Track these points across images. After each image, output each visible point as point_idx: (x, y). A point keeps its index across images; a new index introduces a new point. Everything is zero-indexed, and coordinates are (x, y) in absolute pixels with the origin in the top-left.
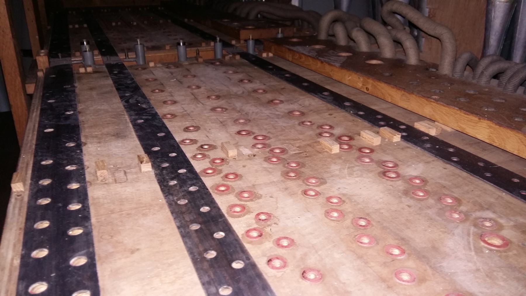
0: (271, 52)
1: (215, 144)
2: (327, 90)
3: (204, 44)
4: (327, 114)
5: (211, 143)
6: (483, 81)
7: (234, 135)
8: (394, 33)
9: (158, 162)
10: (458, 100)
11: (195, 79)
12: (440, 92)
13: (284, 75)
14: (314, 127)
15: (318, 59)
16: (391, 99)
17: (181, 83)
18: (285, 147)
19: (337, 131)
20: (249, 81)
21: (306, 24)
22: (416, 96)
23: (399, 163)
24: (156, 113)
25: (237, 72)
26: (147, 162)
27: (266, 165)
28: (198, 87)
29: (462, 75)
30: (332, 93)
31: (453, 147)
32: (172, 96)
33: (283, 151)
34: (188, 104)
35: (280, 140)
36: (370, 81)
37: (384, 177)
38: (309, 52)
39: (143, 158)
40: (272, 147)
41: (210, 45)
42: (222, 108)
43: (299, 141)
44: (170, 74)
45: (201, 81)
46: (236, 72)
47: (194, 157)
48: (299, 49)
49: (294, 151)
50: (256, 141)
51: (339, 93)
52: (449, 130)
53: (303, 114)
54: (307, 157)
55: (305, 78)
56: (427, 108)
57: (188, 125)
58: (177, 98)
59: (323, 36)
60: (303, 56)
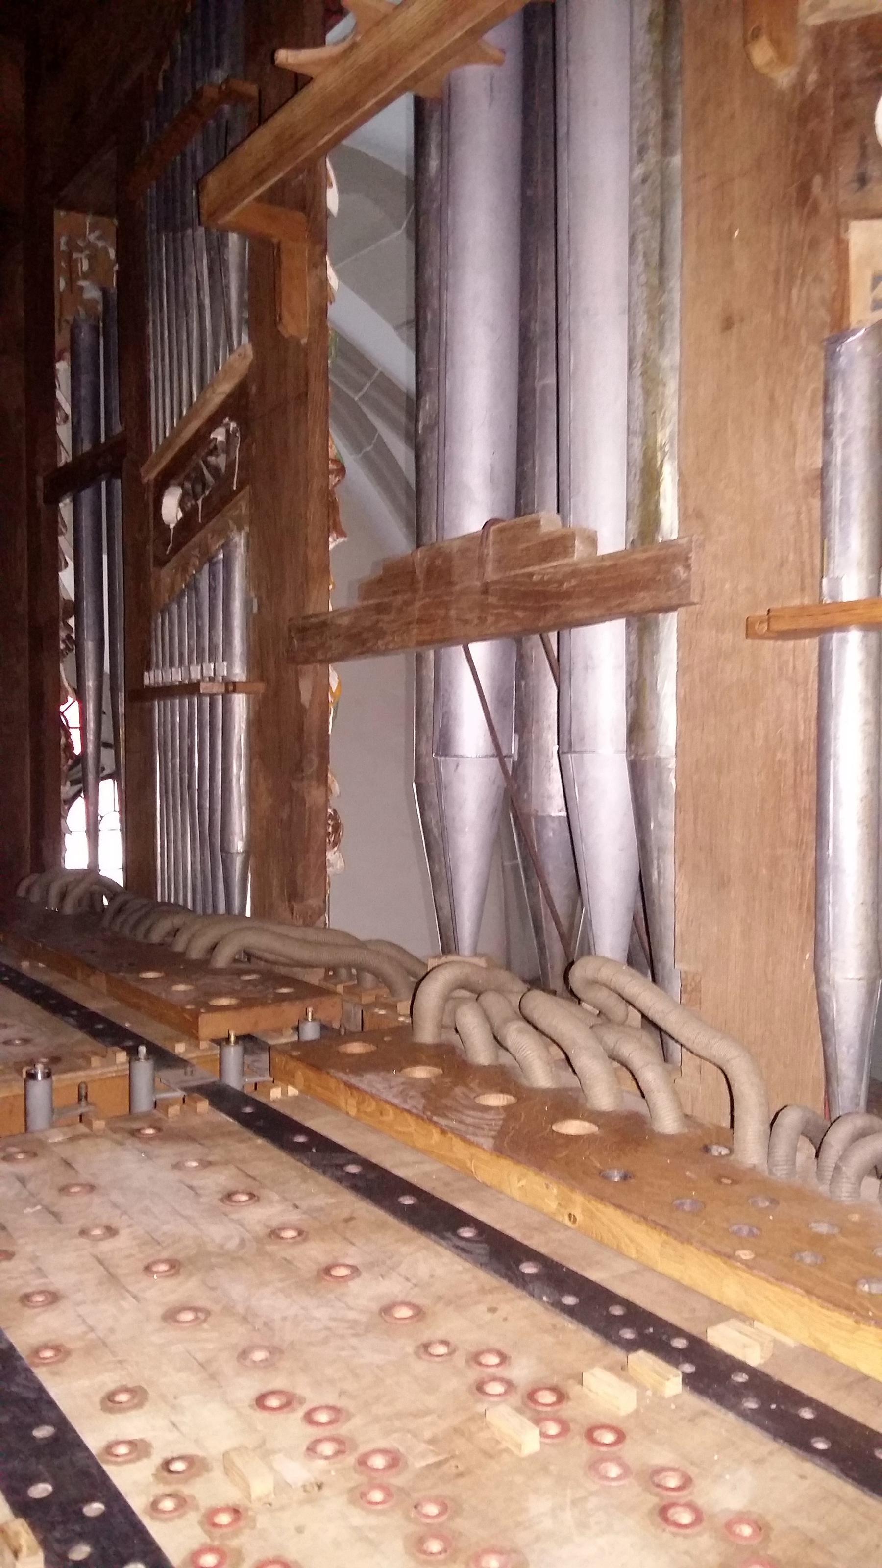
0: (293, 1085)
1: (201, 1453)
2: (467, 1220)
3: (95, 1061)
4: (482, 1308)
5: (191, 1449)
6: (844, 1191)
7: (249, 1411)
8: (611, 1038)
9: (58, 1541)
10: (797, 1258)
11: (96, 1199)
12: (751, 1231)
13: (341, 1167)
14: (460, 1360)
15: (430, 1120)
16: (638, 1252)
17: (57, 1216)
18: (396, 1445)
19: (522, 1371)
20: (252, 1196)
21: (369, 978)
22: (698, 1249)
23: (693, 1471)
24: (11, 1348)
25: (210, 1164)
26: (32, 1553)
27: (357, 1517)
28: (111, 1231)
29: (792, 1171)
30: (484, 1230)
31: (809, 1402)
32: (40, 1272)
33: (395, 1461)
34: (96, 1302)
35: (377, 1419)
36: (578, 1198)
37: (664, 1525)
38: (403, 1094)
39: (17, 1534)
40: (363, 1449)
41: (114, 1062)
42: (195, 1310)
43: (428, 1419)
44: (18, 1184)
45: (115, 1206)
46: (206, 1164)
47: (154, 1506)
48: (370, 1081)
49: (423, 1456)
50: (315, 1432)
51: (498, 1227)
52: (790, 1342)
53: (419, 1313)
54: (460, 1475)
55: (401, 1172)
56: (730, 1285)
57: (112, 1386)
58: (58, 1281)
59: (427, 1034)
60: (387, 1107)
